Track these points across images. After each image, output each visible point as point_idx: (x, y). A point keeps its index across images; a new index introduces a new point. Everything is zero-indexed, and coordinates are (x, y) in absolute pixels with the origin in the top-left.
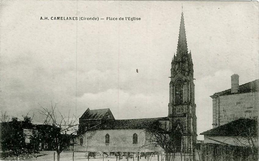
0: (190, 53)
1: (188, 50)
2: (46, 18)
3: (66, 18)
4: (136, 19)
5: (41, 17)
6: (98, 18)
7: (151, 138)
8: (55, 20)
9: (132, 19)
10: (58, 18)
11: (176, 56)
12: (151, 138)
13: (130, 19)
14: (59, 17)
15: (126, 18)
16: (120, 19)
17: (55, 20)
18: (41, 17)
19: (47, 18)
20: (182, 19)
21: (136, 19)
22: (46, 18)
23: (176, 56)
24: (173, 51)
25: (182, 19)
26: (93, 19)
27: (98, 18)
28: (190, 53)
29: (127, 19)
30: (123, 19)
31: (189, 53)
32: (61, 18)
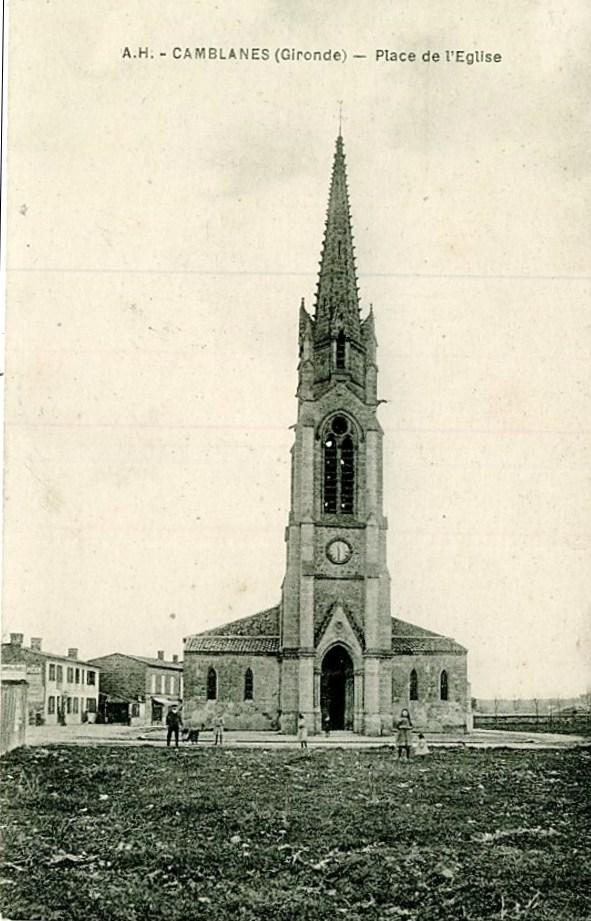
0: (371, 316)
1: (361, 304)
2: (143, 50)
3: (226, 54)
4: (484, 58)
5: (127, 49)
6: (278, 61)
7: (365, 360)
8: (127, 57)
9: (470, 58)
10: (200, 52)
11: (311, 311)
12: (365, 360)
13: (464, 58)
14: (203, 49)
15: (448, 52)
16: (426, 57)
17: (127, 57)
18: (127, 49)
19: (146, 52)
20: (340, 157)
21: (484, 58)
22: (143, 55)
23: (311, 311)
24: (303, 288)
25: (340, 157)
26: (327, 56)
27: (278, 61)
28: (371, 316)
29: (453, 58)
30: (436, 57)
31: (363, 315)
32: (210, 54)
